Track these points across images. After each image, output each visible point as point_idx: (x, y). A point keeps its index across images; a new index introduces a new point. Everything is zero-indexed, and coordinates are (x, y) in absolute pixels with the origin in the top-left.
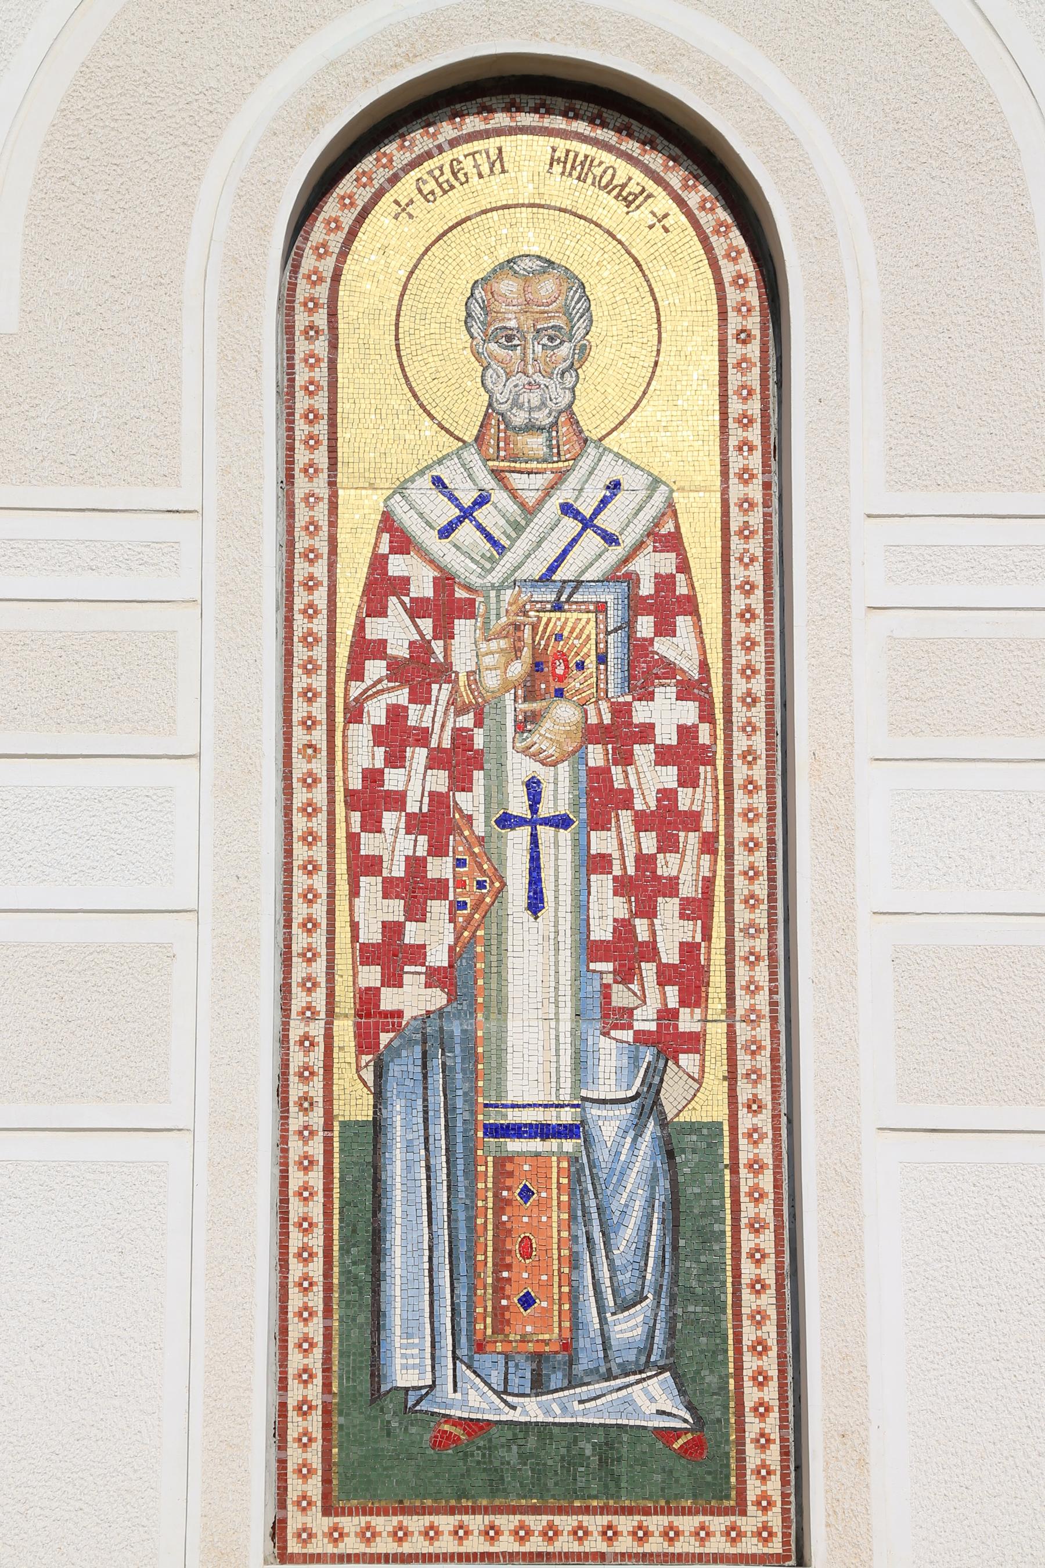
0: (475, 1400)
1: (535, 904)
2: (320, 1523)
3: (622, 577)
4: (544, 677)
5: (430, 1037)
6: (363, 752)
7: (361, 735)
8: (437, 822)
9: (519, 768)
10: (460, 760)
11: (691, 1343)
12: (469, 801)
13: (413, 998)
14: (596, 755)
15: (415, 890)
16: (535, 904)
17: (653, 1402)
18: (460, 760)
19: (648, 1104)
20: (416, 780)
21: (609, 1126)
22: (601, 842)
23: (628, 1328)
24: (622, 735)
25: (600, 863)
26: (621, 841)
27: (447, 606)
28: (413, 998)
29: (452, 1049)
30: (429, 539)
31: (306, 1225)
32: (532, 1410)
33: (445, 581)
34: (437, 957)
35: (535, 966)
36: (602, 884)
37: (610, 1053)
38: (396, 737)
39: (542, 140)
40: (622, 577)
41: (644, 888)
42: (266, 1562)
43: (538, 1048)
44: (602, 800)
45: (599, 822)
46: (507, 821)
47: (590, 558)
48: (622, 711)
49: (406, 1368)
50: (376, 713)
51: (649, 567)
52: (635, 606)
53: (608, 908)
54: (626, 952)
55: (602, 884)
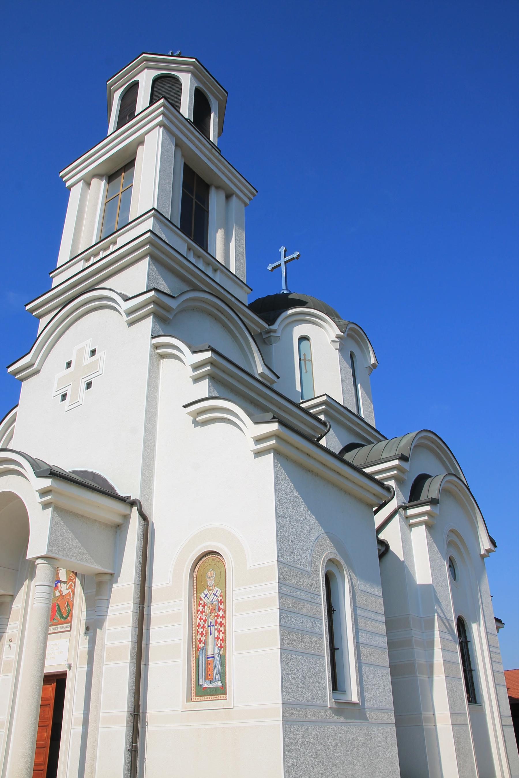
0: (206, 685)
1: (211, 634)
2: (195, 698)
3: (218, 600)
4: (211, 612)
5: (203, 649)
6: (198, 621)
7: (198, 619)
8: (203, 627)
9: (210, 620)
10: (205, 621)
11: (223, 678)
12: (206, 625)
13: (202, 645)
14: (216, 618)
15: (202, 634)
16: (211, 634)
17: (219, 684)
18: (205, 621)
19: (219, 653)
20: (202, 623)
21: (216, 656)
22: (216, 627)
23: (217, 677)
24: (218, 616)
25: (216, 629)
26: (217, 627)
27: (204, 606)
28: (202, 645)
29: (205, 649)
30: (203, 598)
31: (198, 699)
32: (210, 686)
33: (204, 603)
34: (203, 641)
35: (211, 639)
36: (216, 631)
37: (216, 648)
38: (201, 619)
39: (306, 400)
40: (218, 600)
41: (219, 631)
42: (189, 700)
43: (211, 650)
44: (216, 622)
45: (216, 625)
46: (209, 626)
47: (216, 598)
48: (218, 614)
49: (201, 683)
50: (199, 617)
51: (220, 598)
52: (219, 602)
53: (216, 634)
54: (218, 638)
55: (216, 631)
